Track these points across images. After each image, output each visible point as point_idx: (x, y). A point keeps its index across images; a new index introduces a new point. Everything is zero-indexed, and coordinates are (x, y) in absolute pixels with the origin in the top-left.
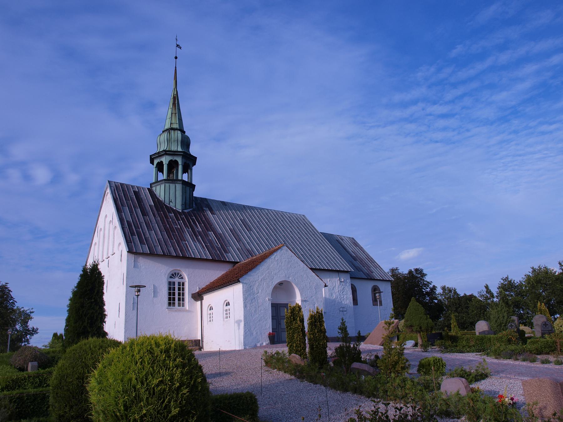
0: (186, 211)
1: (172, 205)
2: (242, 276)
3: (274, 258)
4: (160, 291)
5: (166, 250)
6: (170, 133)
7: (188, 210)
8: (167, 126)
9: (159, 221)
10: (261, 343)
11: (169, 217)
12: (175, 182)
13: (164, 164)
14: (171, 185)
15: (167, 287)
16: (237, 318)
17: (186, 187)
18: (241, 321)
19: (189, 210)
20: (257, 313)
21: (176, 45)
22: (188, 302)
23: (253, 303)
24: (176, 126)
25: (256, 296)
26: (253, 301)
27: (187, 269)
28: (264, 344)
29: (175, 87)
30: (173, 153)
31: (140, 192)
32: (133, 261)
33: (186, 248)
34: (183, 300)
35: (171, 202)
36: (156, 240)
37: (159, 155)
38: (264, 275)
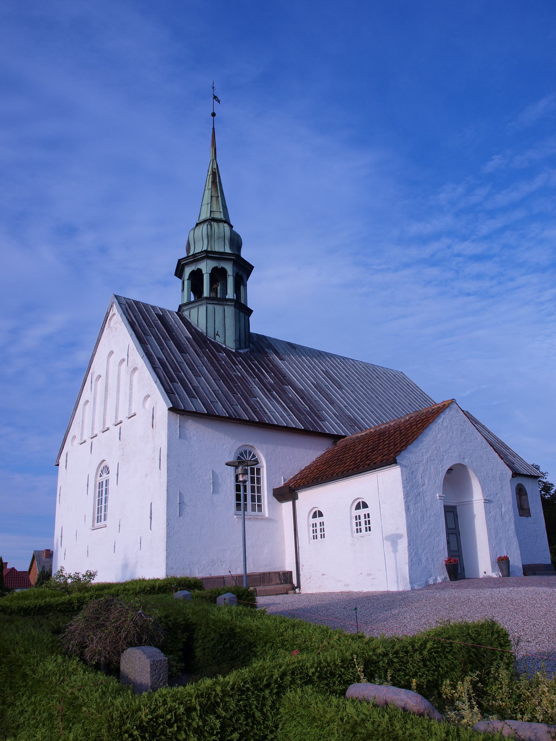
0: (241, 351)
1: (219, 340)
2: (398, 452)
3: (441, 423)
4: (223, 483)
5: (231, 410)
6: (211, 225)
7: (244, 350)
8: (205, 215)
9: (206, 363)
10: (434, 577)
11: (221, 359)
12: (223, 303)
13: (203, 273)
14: (217, 307)
15: (233, 475)
16: (391, 530)
17: (239, 312)
18: (400, 536)
19: (246, 350)
20: (425, 521)
21: (212, 96)
22: (268, 504)
23: (418, 503)
24: (219, 216)
25: (421, 489)
26: (418, 498)
27: (264, 445)
28: (439, 580)
29: (213, 158)
30: (219, 256)
31: (166, 316)
32: (178, 425)
33: (260, 408)
34: (259, 499)
35: (217, 335)
36: (210, 392)
37: (195, 258)
38: (430, 452)
